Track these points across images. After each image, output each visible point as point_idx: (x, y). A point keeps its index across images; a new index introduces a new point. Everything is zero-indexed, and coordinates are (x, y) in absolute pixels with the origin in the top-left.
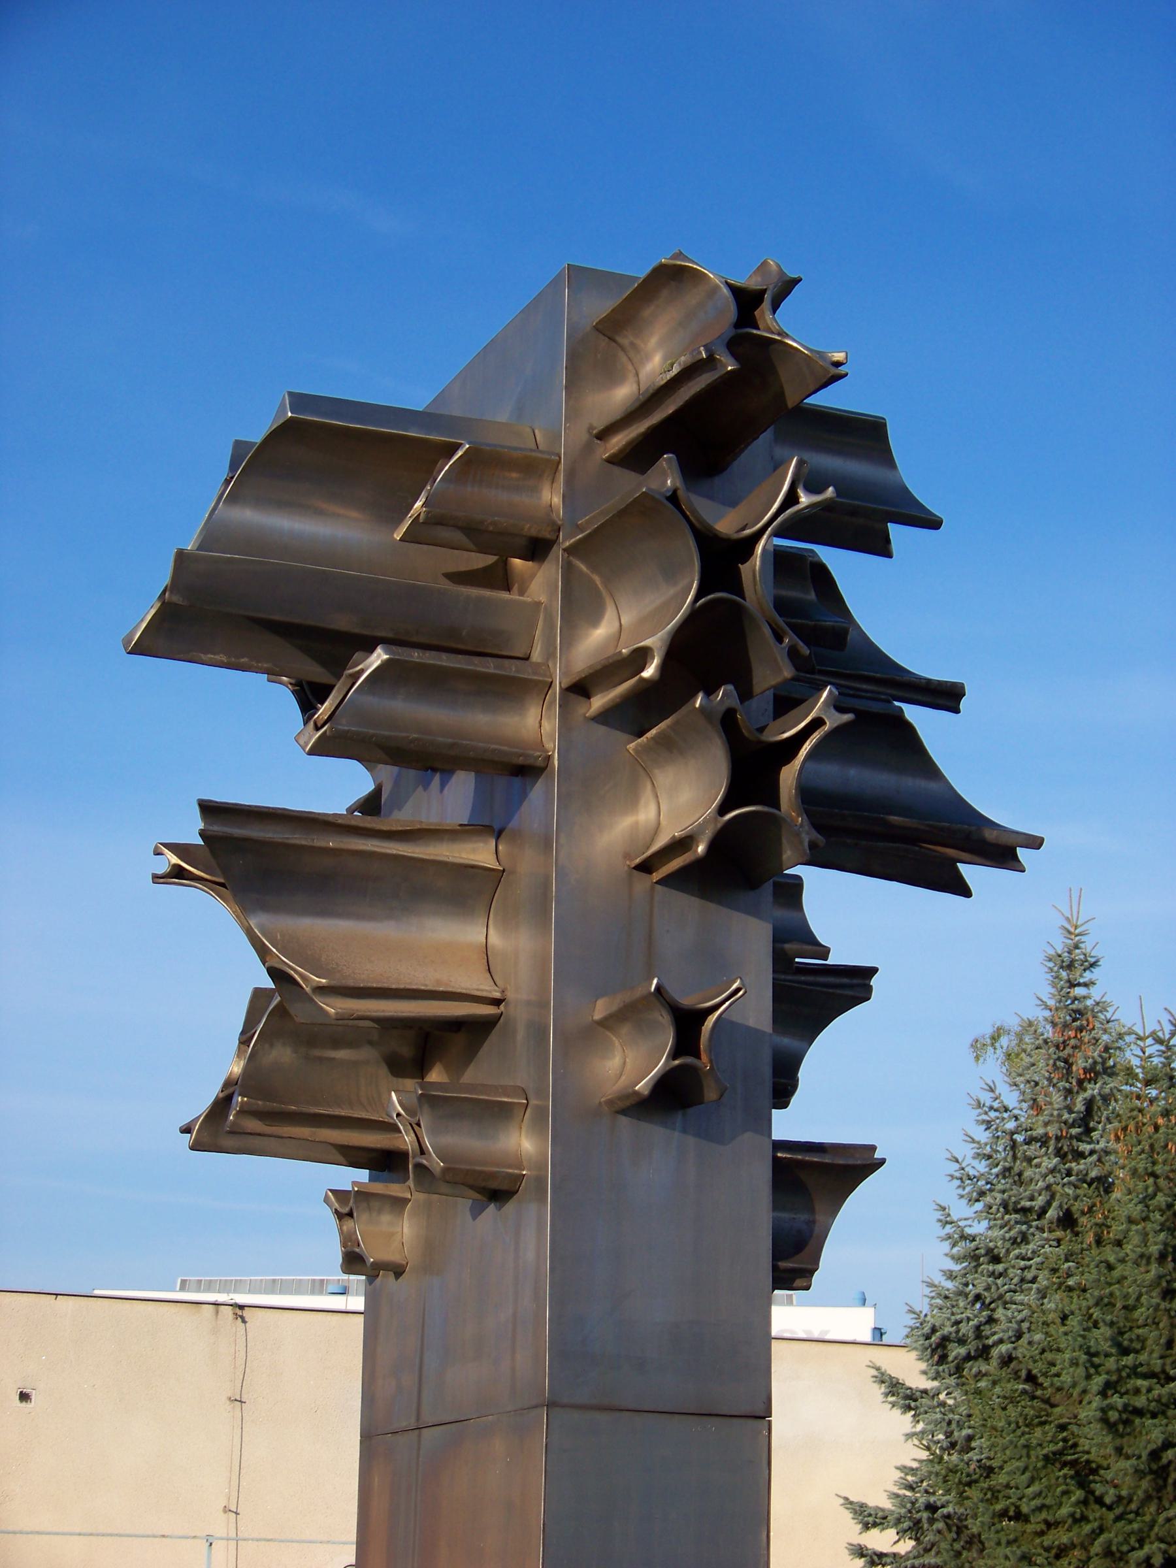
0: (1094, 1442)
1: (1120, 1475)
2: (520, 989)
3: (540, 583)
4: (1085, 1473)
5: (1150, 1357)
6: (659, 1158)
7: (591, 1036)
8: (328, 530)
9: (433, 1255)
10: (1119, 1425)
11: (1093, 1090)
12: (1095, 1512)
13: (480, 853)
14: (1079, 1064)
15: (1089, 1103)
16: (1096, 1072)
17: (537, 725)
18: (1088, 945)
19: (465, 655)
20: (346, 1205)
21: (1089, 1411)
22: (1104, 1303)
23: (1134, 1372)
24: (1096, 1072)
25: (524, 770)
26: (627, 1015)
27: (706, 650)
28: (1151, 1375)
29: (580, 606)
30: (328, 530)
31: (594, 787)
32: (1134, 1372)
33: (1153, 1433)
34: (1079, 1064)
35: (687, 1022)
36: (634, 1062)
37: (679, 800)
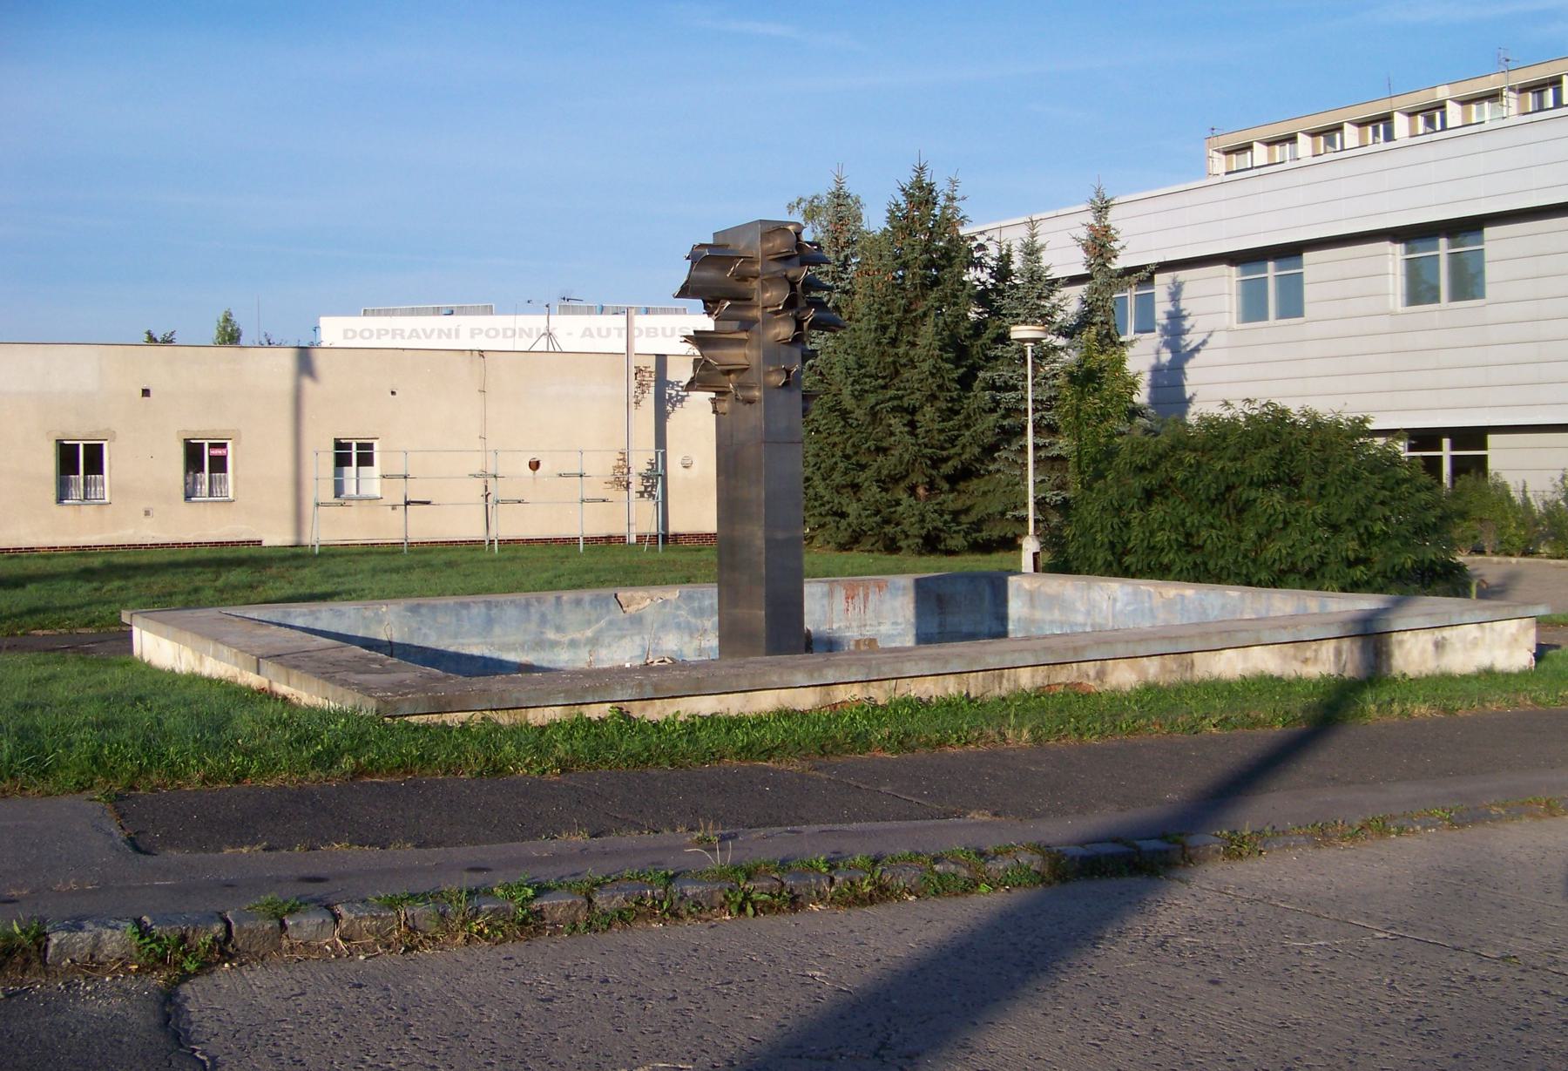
0: (848, 403)
1: (860, 414)
2: (754, 363)
3: (756, 284)
4: (845, 415)
5: (871, 370)
6: (782, 396)
7: (768, 373)
8: (709, 274)
9: (732, 412)
10: (859, 397)
11: (847, 251)
12: (848, 430)
13: (743, 336)
14: (842, 241)
15: (846, 257)
16: (849, 243)
17: (757, 313)
18: (846, 188)
19: (742, 299)
20: (713, 401)
21: (847, 391)
22: (853, 347)
23: (865, 376)
24: (849, 243)
25: (754, 321)
26: (778, 371)
27: (790, 303)
28: (871, 376)
29: (764, 289)
30: (709, 274)
31: (767, 323)
32: (865, 376)
33: (871, 399)
34: (842, 241)
35: (788, 372)
36: (778, 379)
37: (784, 330)
